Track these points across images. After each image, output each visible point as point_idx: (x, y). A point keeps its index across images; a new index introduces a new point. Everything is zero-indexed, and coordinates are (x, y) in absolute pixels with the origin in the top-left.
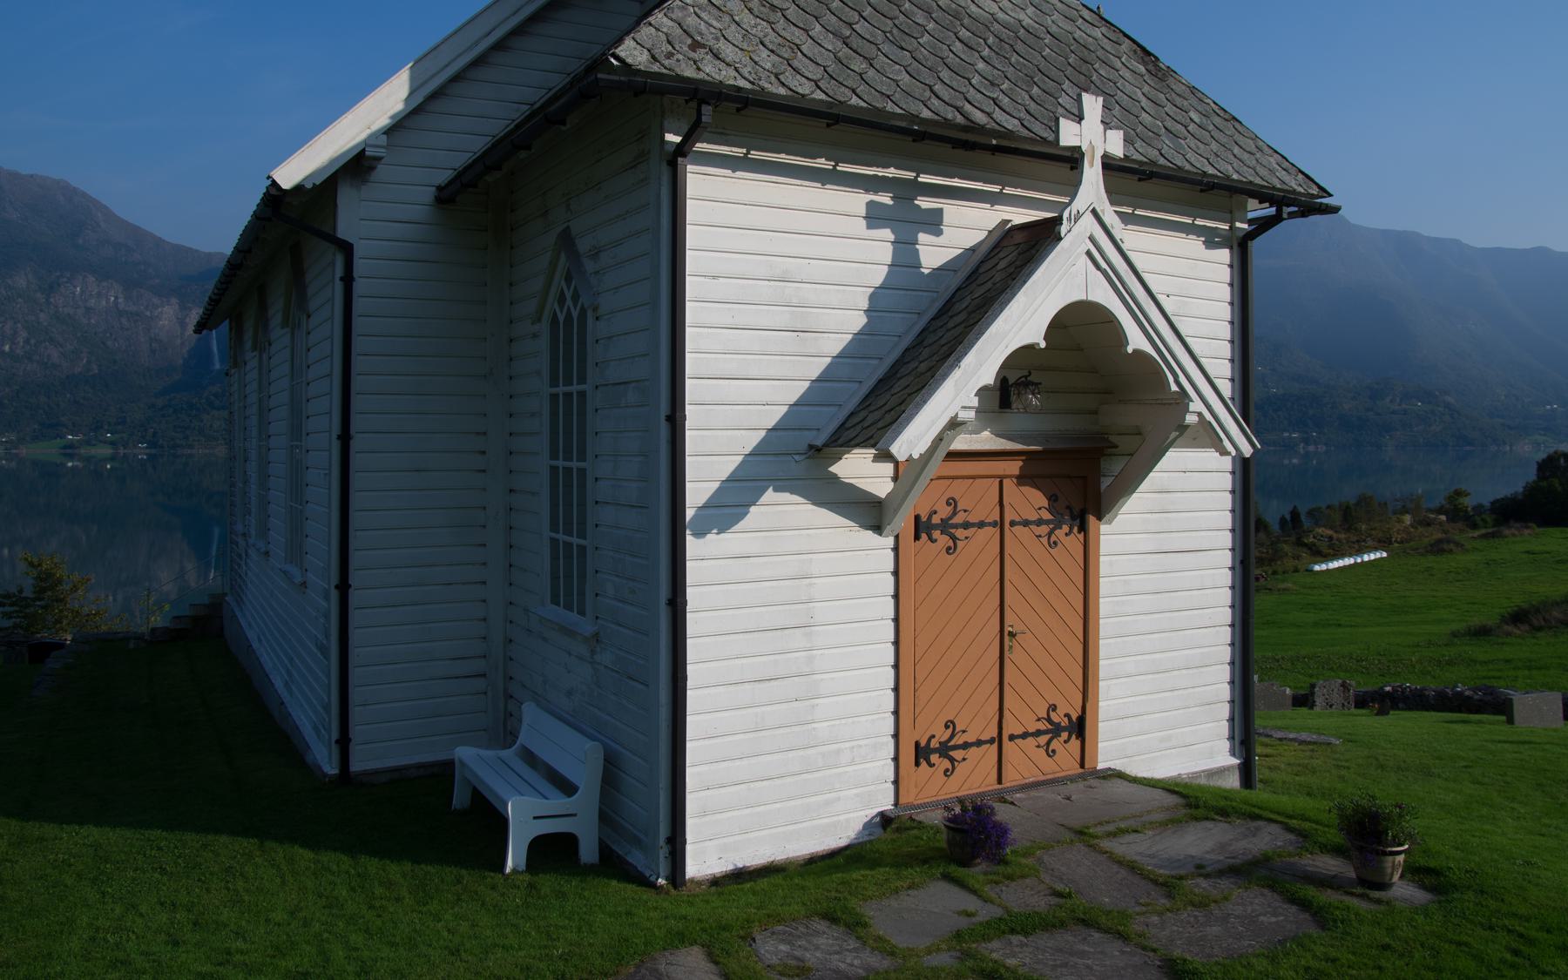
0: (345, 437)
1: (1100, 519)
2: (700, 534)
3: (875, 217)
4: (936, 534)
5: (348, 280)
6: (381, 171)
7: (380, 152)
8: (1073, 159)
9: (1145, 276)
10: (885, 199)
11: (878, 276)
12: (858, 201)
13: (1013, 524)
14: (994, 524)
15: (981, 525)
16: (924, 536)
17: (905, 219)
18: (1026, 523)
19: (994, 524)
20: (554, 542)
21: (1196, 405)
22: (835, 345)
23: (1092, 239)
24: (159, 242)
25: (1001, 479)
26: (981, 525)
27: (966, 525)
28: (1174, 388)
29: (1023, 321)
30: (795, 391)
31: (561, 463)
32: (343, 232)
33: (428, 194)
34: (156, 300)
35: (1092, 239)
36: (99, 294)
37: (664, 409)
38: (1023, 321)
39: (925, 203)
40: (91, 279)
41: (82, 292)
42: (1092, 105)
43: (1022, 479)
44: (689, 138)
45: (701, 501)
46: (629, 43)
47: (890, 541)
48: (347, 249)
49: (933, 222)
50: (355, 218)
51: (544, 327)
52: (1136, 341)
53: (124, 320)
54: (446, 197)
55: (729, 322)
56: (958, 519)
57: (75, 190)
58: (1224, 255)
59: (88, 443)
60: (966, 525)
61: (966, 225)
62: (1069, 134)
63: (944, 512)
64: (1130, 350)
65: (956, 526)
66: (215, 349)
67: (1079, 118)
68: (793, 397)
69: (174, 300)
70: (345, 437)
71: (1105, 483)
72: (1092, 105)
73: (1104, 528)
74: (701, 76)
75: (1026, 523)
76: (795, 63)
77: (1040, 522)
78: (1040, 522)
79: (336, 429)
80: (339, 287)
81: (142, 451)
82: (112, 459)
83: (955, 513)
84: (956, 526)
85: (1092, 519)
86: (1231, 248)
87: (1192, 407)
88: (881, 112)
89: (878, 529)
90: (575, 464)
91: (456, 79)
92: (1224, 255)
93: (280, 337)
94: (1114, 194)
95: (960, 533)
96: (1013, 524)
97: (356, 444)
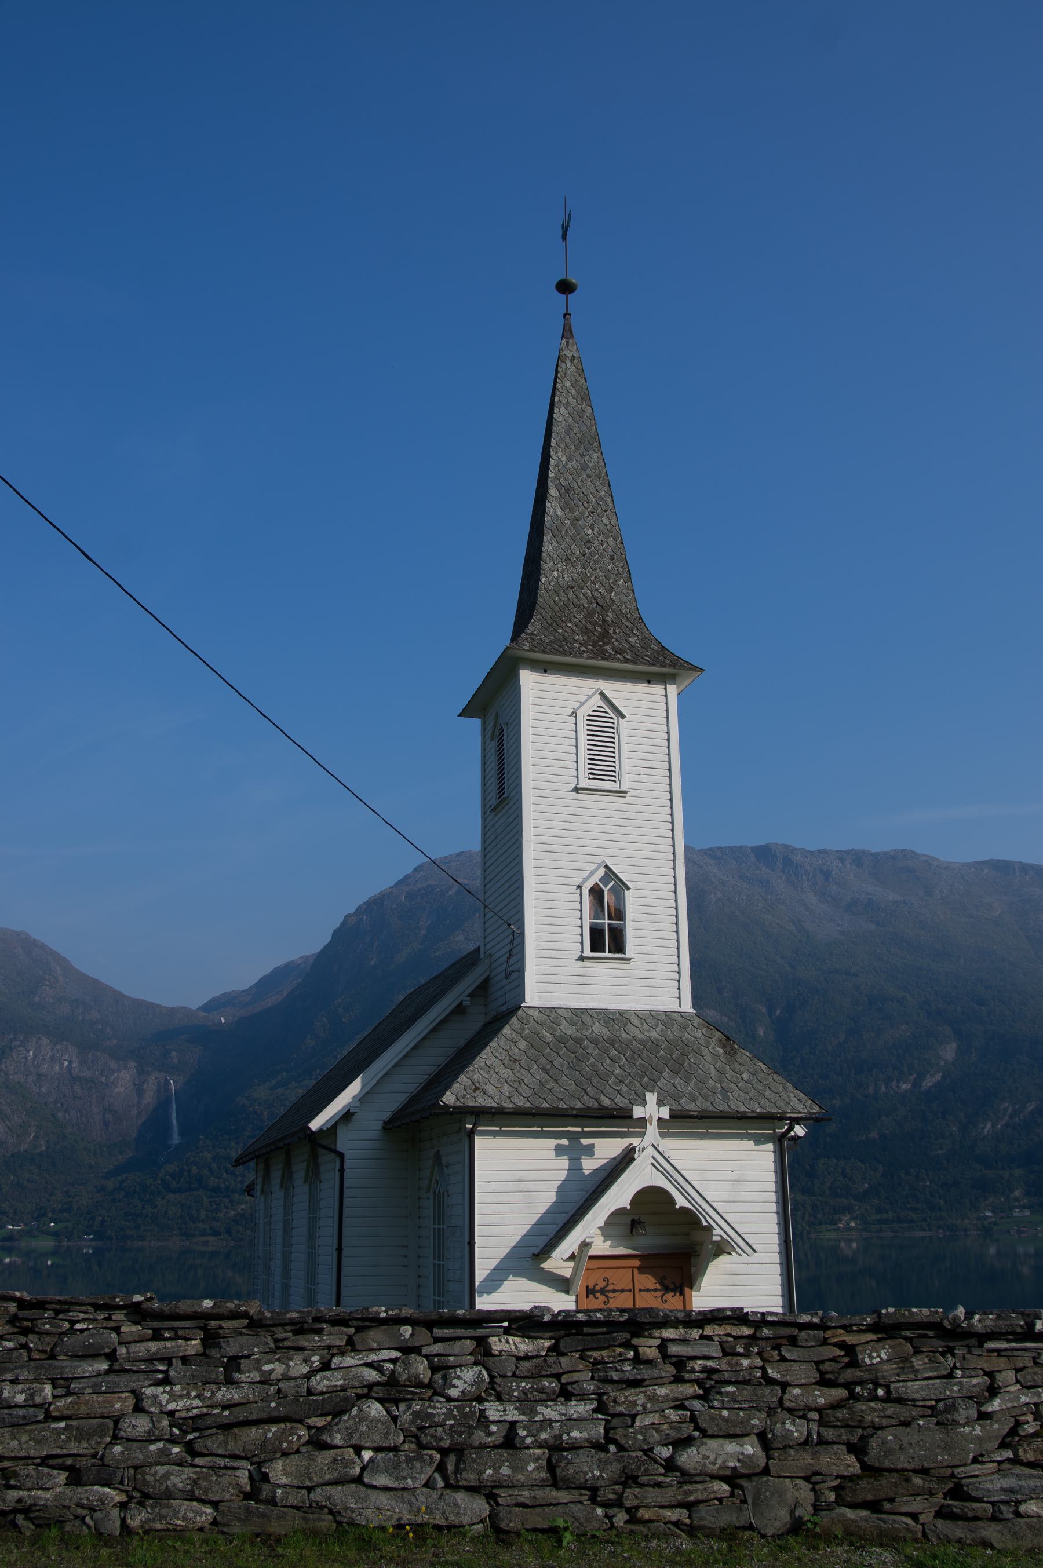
0: (340, 1249)
1: (691, 1288)
2: (481, 1295)
3: (559, 1151)
4: (598, 1295)
5: (342, 1170)
6: (356, 1117)
7: (357, 1110)
8: (643, 1122)
9: (682, 1172)
10: (565, 1142)
11: (563, 1175)
12: (552, 1143)
13: (640, 1290)
14: (630, 1291)
15: (622, 1291)
16: (591, 1296)
17: (575, 1152)
18: (648, 1290)
19: (630, 1291)
20: (434, 1300)
21: (717, 1232)
22: (543, 1208)
23: (653, 1158)
24: (119, 997)
25: (633, 1268)
26: (622, 1291)
27: (614, 1291)
28: (705, 1223)
29: (620, 1195)
30: (524, 1230)
31: (437, 1262)
32: (339, 1149)
33: (379, 1125)
34: (112, 1064)
35: (653, 1158)
36: (52, 1058)
37: (467, 1239)
38: (620, 1195)
39: (585, 1141)
40: (45, 1041)
41: (35, 1056)
42: (651, 1098)
43: (641, 1270)
44: (475, 1125)
45: (482, 1278)
46: (448, 1093)
47: (574, 1298)
48: (341, 1156)
49: (590, 1150)
50: (344, 1142)
51: (431, 1195)
52: (681, 1202)
53: (77, 1088)
54: (390, 1126)
55: (496, 1201)
56: (609, 1288)
57: (35, 942)
58: (770, 1146)
59: (29, 1234)
60: (614, 1291)
61: (606, 1149)
62: (638, 1112)
63: (602, 1284)
64: (677, 1207)
65: (609, 1291)
66: (175, 1122)
67: (644, 1103)
68: (524, 1232)
69: (132, 1064)
70: (340, 1249)
71: (693, 1269)
72: (651, 1098)
73: (694, 1294)
74: (477, 1104)
75: (648, 1290)
76: (520, 1090)
77: (656, 1290)
78: (656, 1290)
79: (335, 1245)
80: (338, 1174)
81: (87, 1245)
82: (54, 1253)
83: (607, 1285)
84: (609, 1291)
85: (687, 1289)
86: (774, 1143)
87: (715, 1232)
88: (557, 1108)
89: (567, 1292)
90: (441, 1262)
91: (396, 1065)
92: (770, 1146)
93: (301, 1191)
94: (663, 1135)
95: (610, 1295)
96: (640, 1290)
97: (345, 1252)
